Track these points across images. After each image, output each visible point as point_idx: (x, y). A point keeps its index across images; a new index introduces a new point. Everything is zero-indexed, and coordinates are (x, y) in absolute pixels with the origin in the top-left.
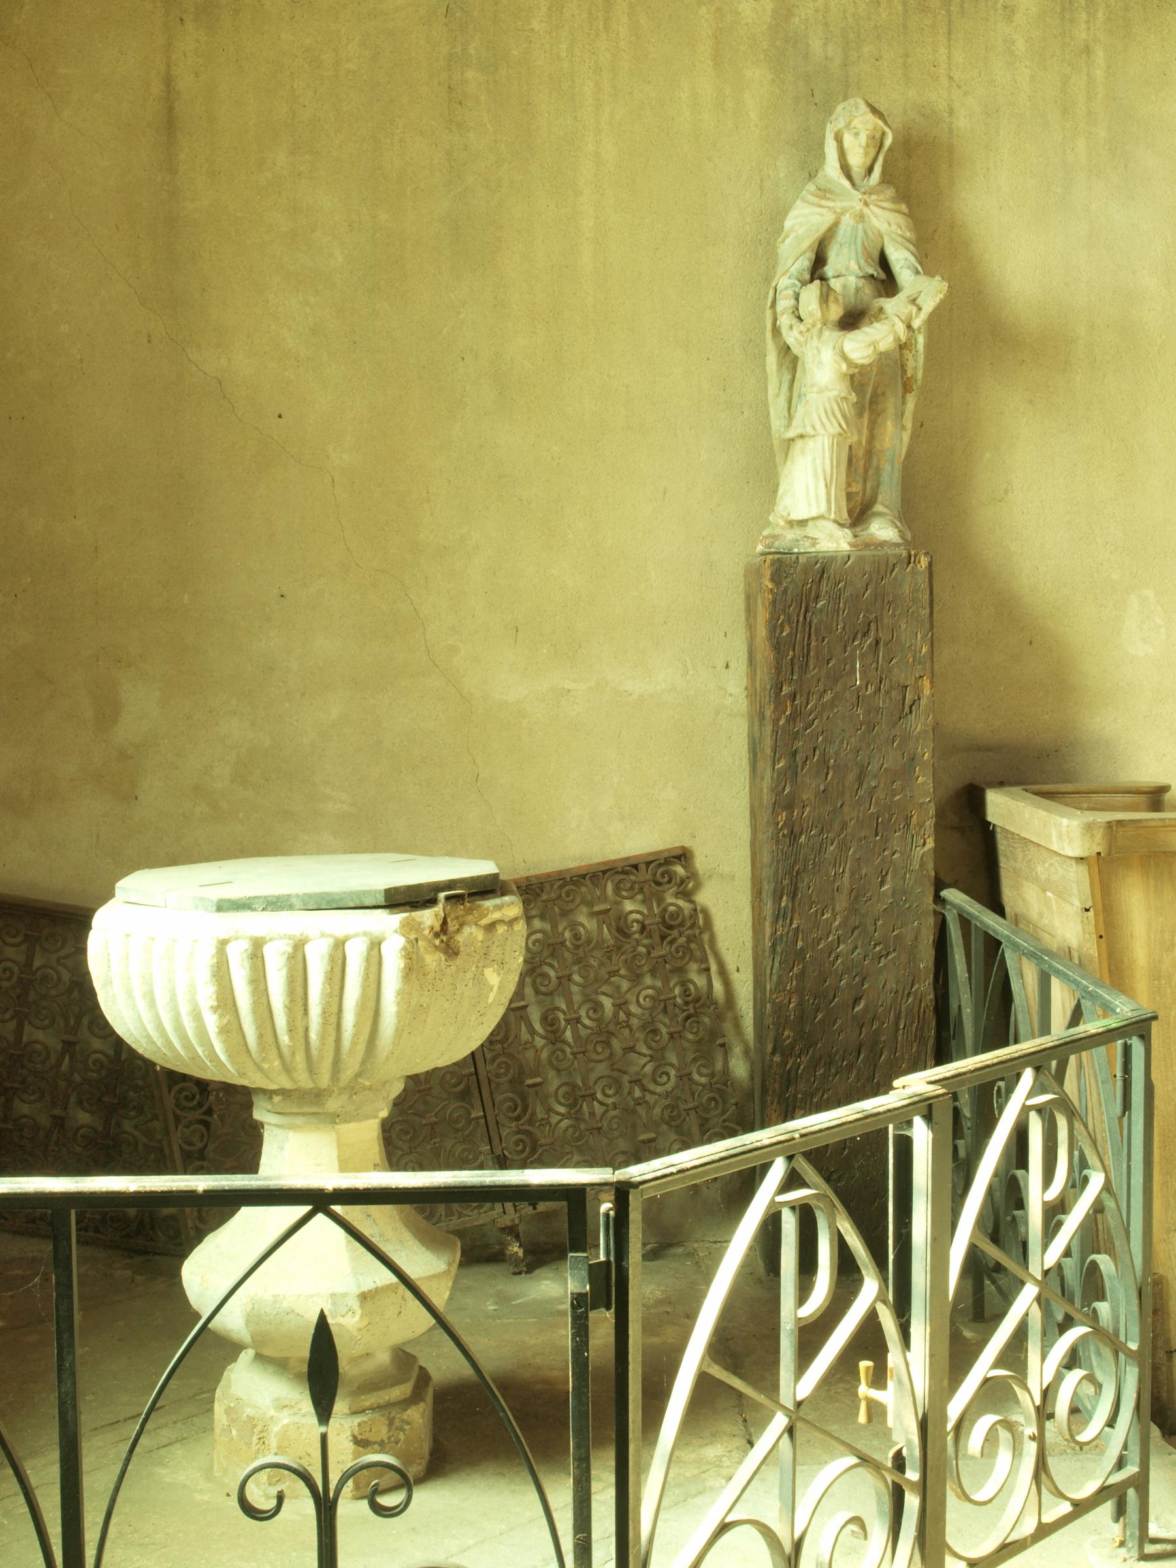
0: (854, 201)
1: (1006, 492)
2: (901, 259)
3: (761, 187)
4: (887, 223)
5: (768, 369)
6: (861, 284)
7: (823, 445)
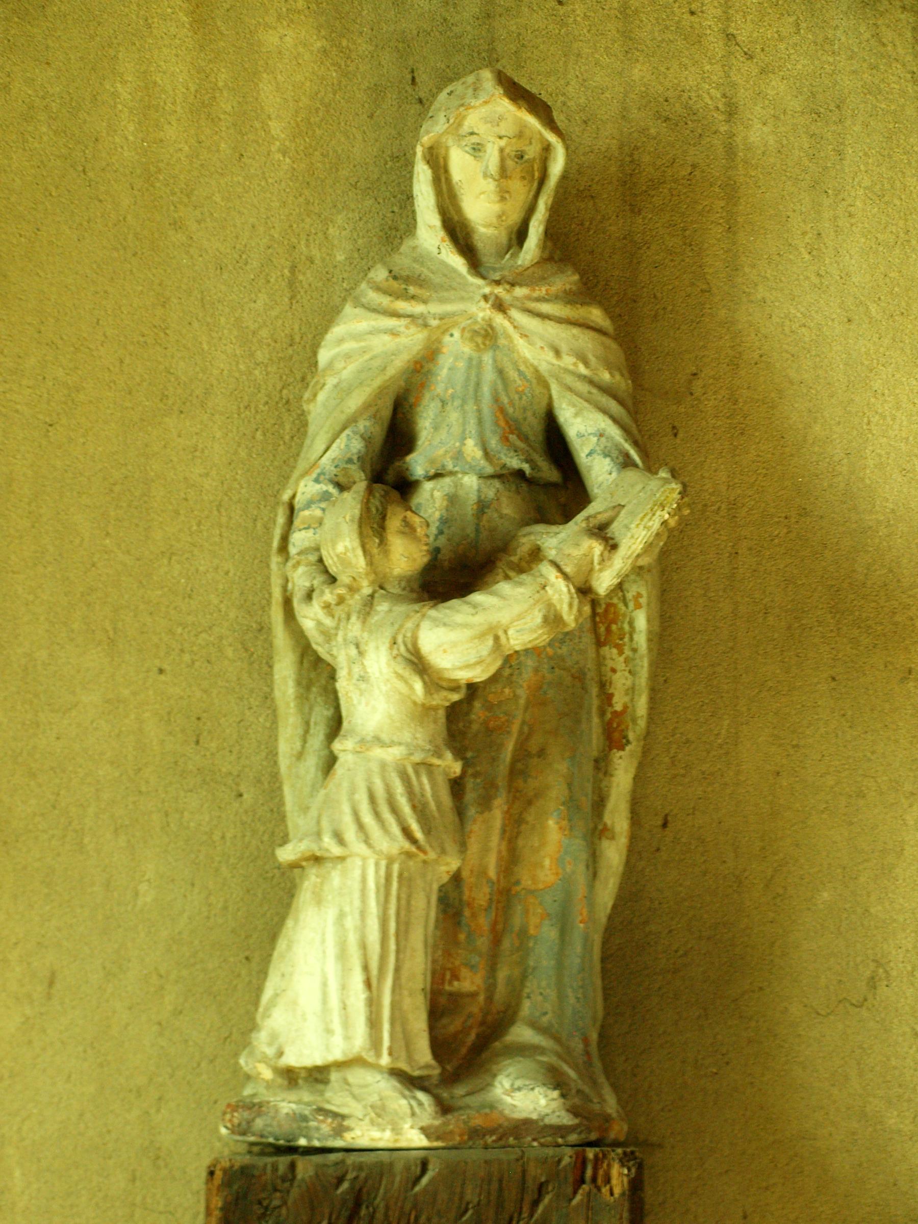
0: (473, 302)
1: (872, 983)
2: (588, 429)
3: (292, 284)
4: (550, 347)
5: (277, 693)
6: (491, 494)
7: (364, 880)
